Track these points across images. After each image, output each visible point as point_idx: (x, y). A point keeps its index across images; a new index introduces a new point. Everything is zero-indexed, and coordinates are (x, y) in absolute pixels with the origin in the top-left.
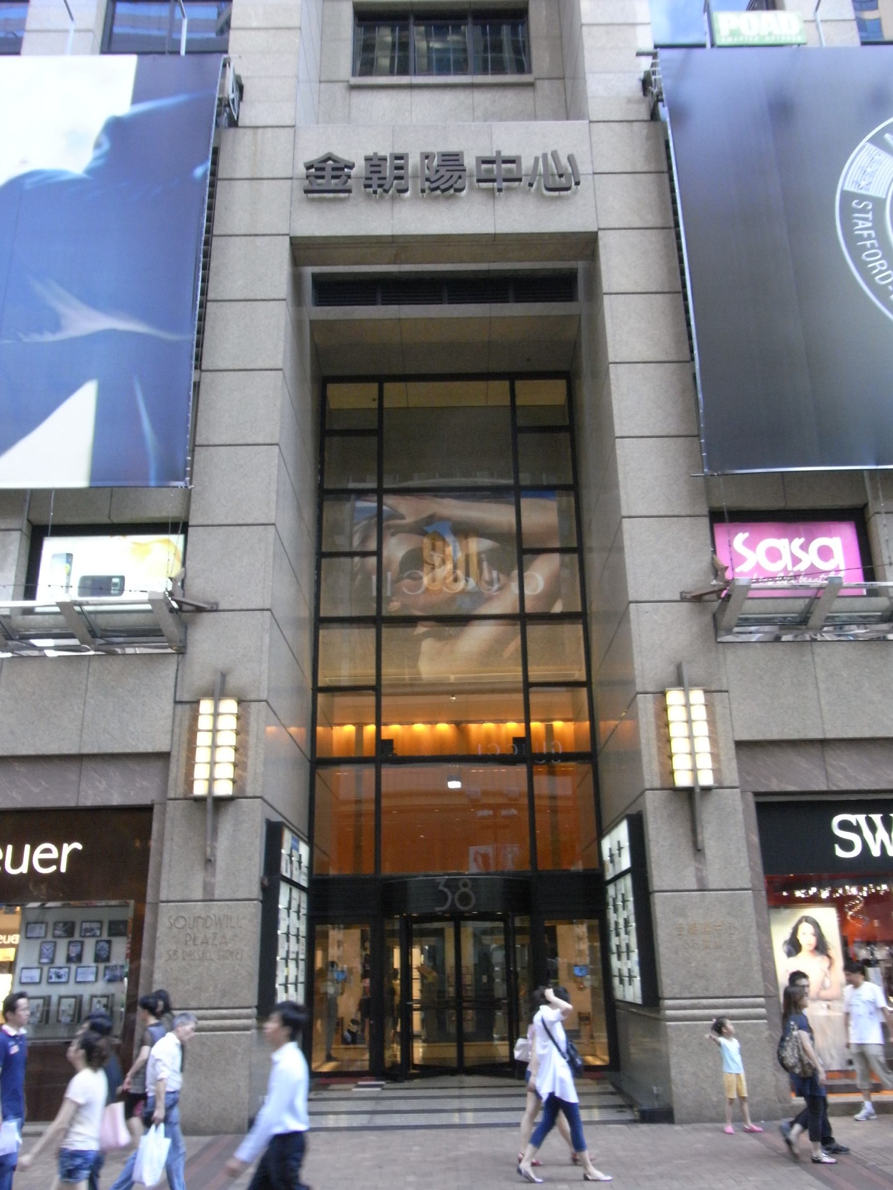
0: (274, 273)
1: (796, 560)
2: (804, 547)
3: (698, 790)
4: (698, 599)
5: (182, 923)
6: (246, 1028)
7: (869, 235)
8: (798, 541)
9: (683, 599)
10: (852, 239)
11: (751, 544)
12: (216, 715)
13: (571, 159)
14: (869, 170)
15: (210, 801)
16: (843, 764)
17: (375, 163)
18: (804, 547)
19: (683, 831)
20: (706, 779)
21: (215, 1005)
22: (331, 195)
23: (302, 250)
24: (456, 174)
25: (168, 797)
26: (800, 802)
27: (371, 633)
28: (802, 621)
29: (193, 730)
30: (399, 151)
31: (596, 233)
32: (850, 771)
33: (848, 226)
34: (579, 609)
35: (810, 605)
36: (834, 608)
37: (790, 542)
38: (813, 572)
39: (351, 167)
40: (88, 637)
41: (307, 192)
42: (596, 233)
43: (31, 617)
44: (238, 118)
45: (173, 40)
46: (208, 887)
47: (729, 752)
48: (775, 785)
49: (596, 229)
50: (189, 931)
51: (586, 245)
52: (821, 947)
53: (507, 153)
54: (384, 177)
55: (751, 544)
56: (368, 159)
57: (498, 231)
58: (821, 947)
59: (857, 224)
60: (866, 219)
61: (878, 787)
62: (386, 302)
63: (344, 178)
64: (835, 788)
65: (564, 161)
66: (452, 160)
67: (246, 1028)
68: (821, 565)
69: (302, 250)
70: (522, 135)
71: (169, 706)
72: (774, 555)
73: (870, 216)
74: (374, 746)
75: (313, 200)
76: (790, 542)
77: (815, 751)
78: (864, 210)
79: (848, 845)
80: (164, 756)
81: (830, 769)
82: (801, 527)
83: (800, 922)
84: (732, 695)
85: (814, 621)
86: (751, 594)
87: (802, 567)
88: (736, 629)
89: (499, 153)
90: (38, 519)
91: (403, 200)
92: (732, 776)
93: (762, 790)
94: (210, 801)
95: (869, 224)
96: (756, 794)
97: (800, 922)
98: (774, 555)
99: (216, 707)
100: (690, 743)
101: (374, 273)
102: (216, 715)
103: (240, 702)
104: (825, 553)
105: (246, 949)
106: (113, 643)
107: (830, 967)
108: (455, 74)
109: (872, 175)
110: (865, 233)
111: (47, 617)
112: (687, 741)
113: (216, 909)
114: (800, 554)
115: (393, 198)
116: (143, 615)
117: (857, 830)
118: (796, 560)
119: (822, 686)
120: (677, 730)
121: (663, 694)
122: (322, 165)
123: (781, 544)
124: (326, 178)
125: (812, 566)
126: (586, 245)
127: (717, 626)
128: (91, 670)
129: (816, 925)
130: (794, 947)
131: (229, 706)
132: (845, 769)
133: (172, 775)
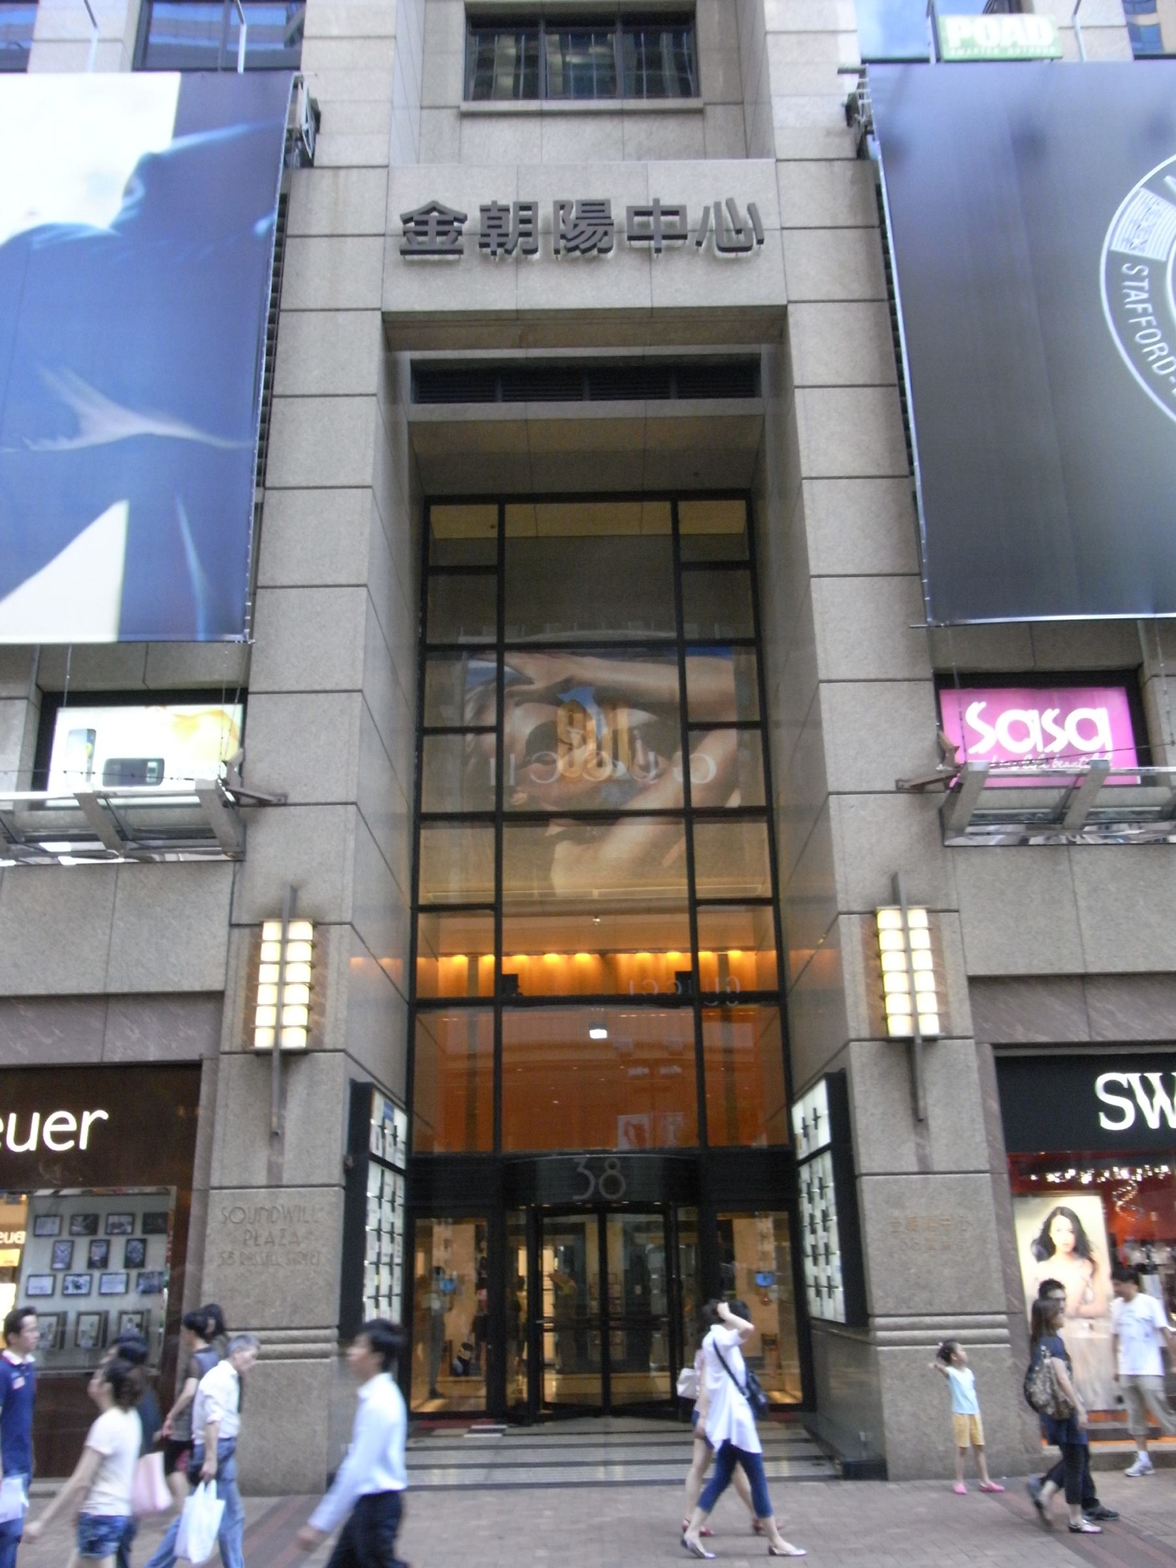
0: (360, 360)
1: (1048, 739)
2: (1059, 721)
3: (919, 1041)
4: (919, 789)
5: (239, 1216)
6: (324, 1355)
7: (1145, 310)
8: (1051, 713)
9: (899, 790)
10: (1122, 315)
11: (989, 717)
12: (284, 942)
13: (752, 210)
14: (1144, 224)
15: (276, 1055)
16: (1110, 1007)
17: (493, 215)
18: (1059, 721)
19: (899, 1095)
20: (930, 1026)
21: (284, 1324)
22: (436, 257)
23: (398, 329)
24: (601, 230)
25: (222, 1050)
26: (1054, 1057)
27: (489, 834)
28: (1056, 818)
29: (254, 963)
30: (525, 199)
31: (785, 307)
32: (1119, 1015)
33: (1117, 298)
34: (762, 802)
35: (1067, 797)
36: (1098, 801)
37: (1041, 714)
38: (1070, 753)
39: (462, 220)
40: (116, 839)
41: (404, 252)
42: (785, 307)
43: (41, 813)
44: (313, 155)
45: (227, 52)
46: (274, 1169)
47: (960, 991)
48: (1020, 1035)
49: (784, 302)
50: (249, 1227)
51: (772, 322)
52: (1081, 1248)
53: (667, 201)
54: (506, 234)
55: (989, 717)
56: (484, 210)
57: (656, 305)
58: (1081, 1248)
59: (1128, 296)
60: (1140, 289)
61: (1156, 1038)
62: (509, 397)
63: (453, 235)
64: (1099, 1039)
65: (743, 212)
66: (595, 211)
67: (324, 1355)
68: (1082, 745)
69: (398, 329)
70: (688, 177)
71: (222, 931)
72: (1019, 731)
73: (1145, 284)
74: (492, 984)
75: (412, 263)
76: (1041, 714)
77: (1073, 990)
78: (1138, 277)
79: (1116, 1114)
80: (216, 997)
81: (1093, 1014)
82: (1055, 694)
83: (1053, 1215)
84: (964, 916)
85: (1072, 818)
86: (989, 782)
87: (1056, 747)
88: (970, 829)
89: (657, 201)
90: (50, 684)
91: (531, 264)
92: (964, 1022)
93: (1003, 1040)
94: (276, 1055)
95: (1145, 296)
96: (996, 1046)
97: (1053, 1215)
98: (1019, 731)
99: (284, 932)
100: (909, 979)
101: (493, 360)
102: (284, 942)
103: (315, 925)
104: (1087, 729)
105: (324, 1250)
106: (148, 848)
107: (1093, 1275)
108: (600, 97)
109: (1148, 231)
110: (1140, 307)
111: (62, 813)
112: (905, 976)
113: (285, 1198)
114: (1053, 729)
115: (517, 261)
116: (189, 811)
117: (1129, 1093)
118: (1048, 739)
119: (1082, 904)
120: (892, 962)
121: (874, 914)
122: (424, 218)
123: (1029, 717)
124: (429, 234)
125: (1070, 746)
126: (772, 322)
127: (944, 825)
128: (120, 883)
129: (1074, 1219)
130: (1045, 1247)
131: (302, 930)
132: (1113, 1013)
133: (227, 1021)
